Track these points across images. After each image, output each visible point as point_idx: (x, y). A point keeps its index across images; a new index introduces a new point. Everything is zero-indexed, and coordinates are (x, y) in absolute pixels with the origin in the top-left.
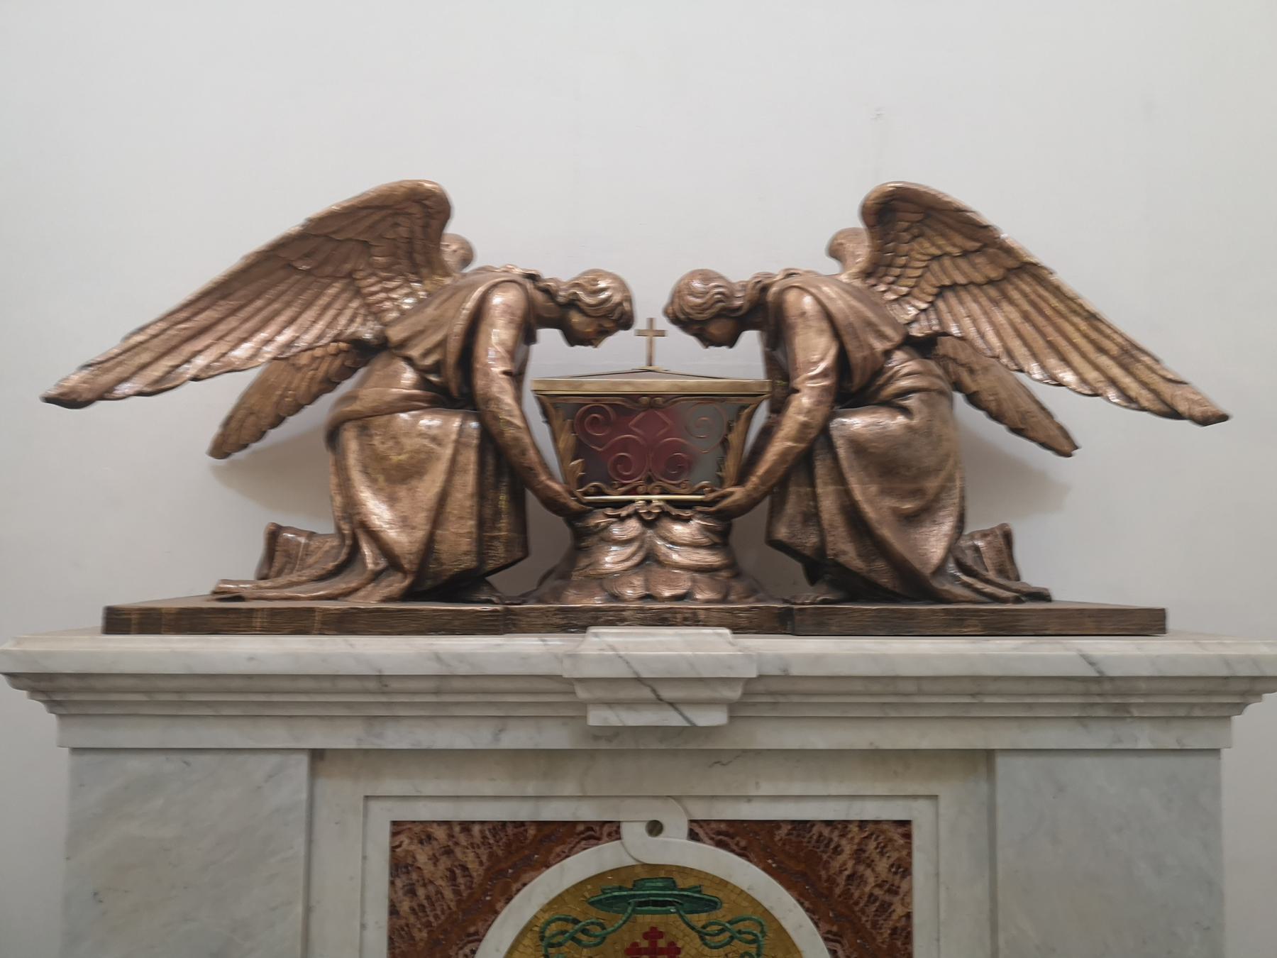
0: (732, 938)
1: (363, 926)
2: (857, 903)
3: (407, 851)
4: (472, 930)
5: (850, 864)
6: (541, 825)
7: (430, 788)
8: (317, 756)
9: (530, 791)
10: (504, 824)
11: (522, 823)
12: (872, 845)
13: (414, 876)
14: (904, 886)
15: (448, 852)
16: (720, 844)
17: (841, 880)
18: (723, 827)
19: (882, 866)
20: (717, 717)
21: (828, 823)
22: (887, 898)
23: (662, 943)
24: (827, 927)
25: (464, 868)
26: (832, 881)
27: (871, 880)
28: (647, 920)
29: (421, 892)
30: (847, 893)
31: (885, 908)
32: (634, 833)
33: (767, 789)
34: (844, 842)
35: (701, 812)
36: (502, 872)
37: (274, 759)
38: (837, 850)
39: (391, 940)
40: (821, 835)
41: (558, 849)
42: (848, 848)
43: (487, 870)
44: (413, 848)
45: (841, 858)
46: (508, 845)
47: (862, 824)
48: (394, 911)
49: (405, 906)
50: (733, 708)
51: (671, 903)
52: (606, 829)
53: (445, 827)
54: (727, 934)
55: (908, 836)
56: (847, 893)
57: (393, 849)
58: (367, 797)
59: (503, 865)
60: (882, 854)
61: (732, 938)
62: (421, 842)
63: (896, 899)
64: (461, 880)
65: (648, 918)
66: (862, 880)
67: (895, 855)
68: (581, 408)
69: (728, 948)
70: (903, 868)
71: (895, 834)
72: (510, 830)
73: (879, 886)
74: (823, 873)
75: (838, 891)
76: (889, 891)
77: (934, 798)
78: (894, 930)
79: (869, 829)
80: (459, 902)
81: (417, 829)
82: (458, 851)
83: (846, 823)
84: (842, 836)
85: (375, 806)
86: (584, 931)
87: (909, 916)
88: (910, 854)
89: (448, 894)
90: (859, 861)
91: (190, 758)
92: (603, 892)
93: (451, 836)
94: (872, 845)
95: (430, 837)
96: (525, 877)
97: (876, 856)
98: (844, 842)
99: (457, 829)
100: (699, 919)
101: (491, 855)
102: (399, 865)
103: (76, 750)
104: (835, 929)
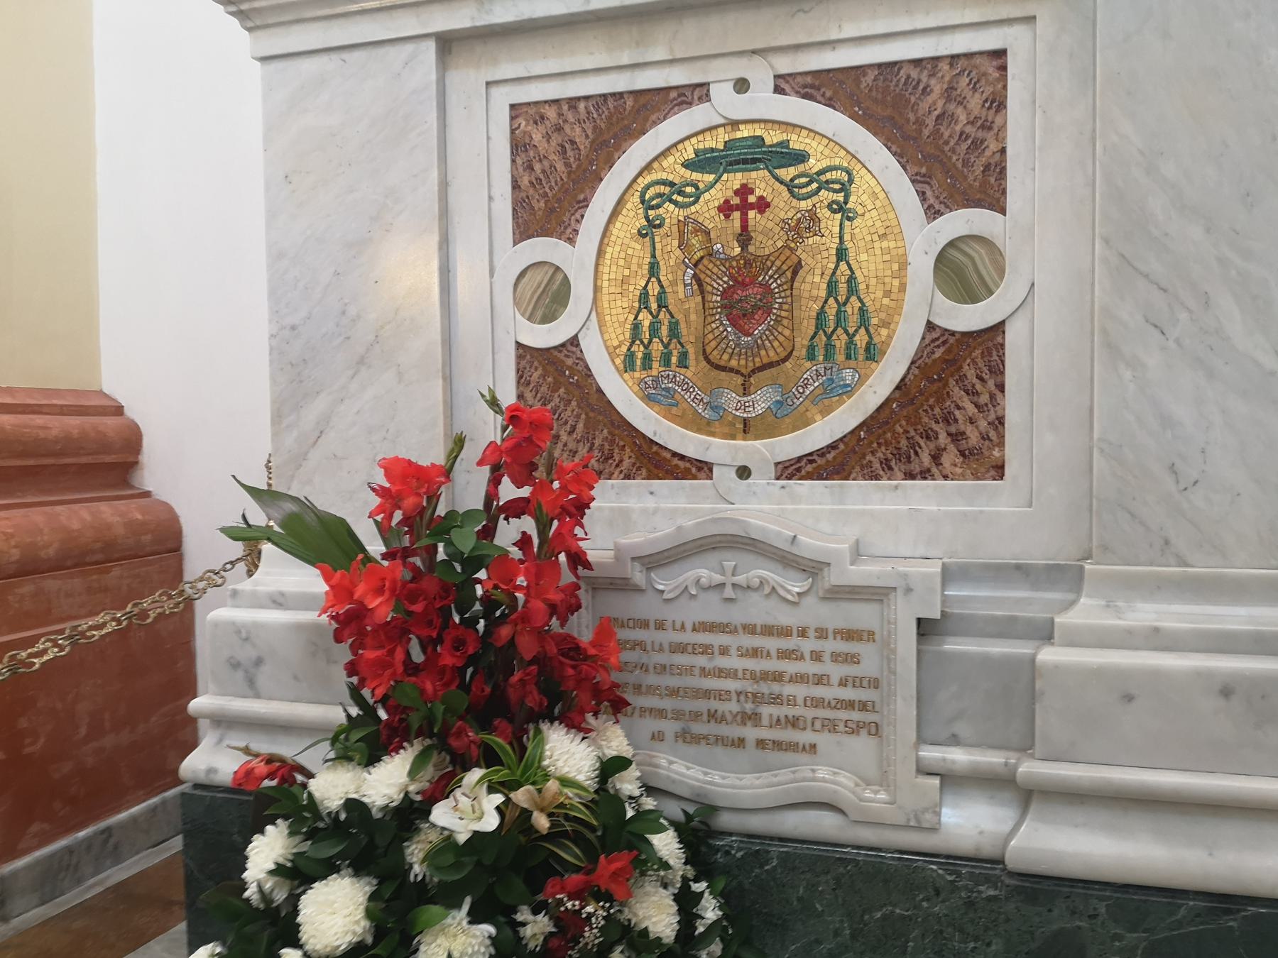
0: (819, 189)
1: (490, 198)
2: (947, 143)
3: (525, 132)
4: (581, 197)
5: (940, 104)
6: (637, 94)
7: (539, 68)
8: (447, 44)
9: (625, 60)
10: (604, 96)
11: (621, 94)
12: (964, 80)
13: (532, 153)
14: (998, 120)
15: (559, 129)
16: (806, 96)
17: (930, 121)
18: (809, 80)
19: (975, 102)
21: (917, 62)
22: (980, 134)
23: (752, 199)
24: (916, 169)
25: (573, 142)
26: (920, 123)
27: (963, 118)
28: (735, 180)
29: (537, 167)
30: (936, 134)
31: (977, 145)
32: (722, 94)
33: (850, 31)
34: (933, 82)
35: (785, 65)
36: (605, 143)
37: (409, 47)
38: (926, 91)
39: (514, 209)
40: (909, 77)
41: (654, 117)
42: (937, 88)
43: (592, 142)
44: (529, 128)
45: (930, 99)
46: (609, 118)
47: (954, 58)
48: (516, 186)
49: (525, 181)
51: (759, 160)
52: (697, 93)
53: (554, 107)
54: (815, 185)
55: (1003, 68)
56: (936, 134)
57: (513, 131)
58: (488, 84)
59: (606, 137)
60: (974, 89)
61: (819, 189)
62: (536, 123)
63: (990, 136)
64: (570, 153)
65: (739, 175)
66: (953, 118)
67: (989, 90)
68: (877, 423)
69: (815, 199)
70: (998, 103)
71: (990, 67)
72: (611, 103)
73: (972, 123)
74: (912, 117)
75: (926, 132)
76: (983, 127)
77: (1031, 19)
78: (987, 167)
79: (961, 64)
80: (569, 173)
81: (532, 111)
82: (567, 128)
83: (936, 59)
84: (931, 75)
85: (495, 91)
86: (680, 193)
87: (1003, 151)
88: (1005, 87)
89: (560, 166)
90: (949, 99)
91: (346, 55)
92: (697, 152)
93: (560, 115)
94: (964, 80)
95: (542, 118)
96: (624, 145)
97: (968, 93)
98: (933, 82)
99: (565, 107)
100: (787, 173)
101: (595, 128)
102: (518, 146)
103: (264, 59)
104: (924, 170)
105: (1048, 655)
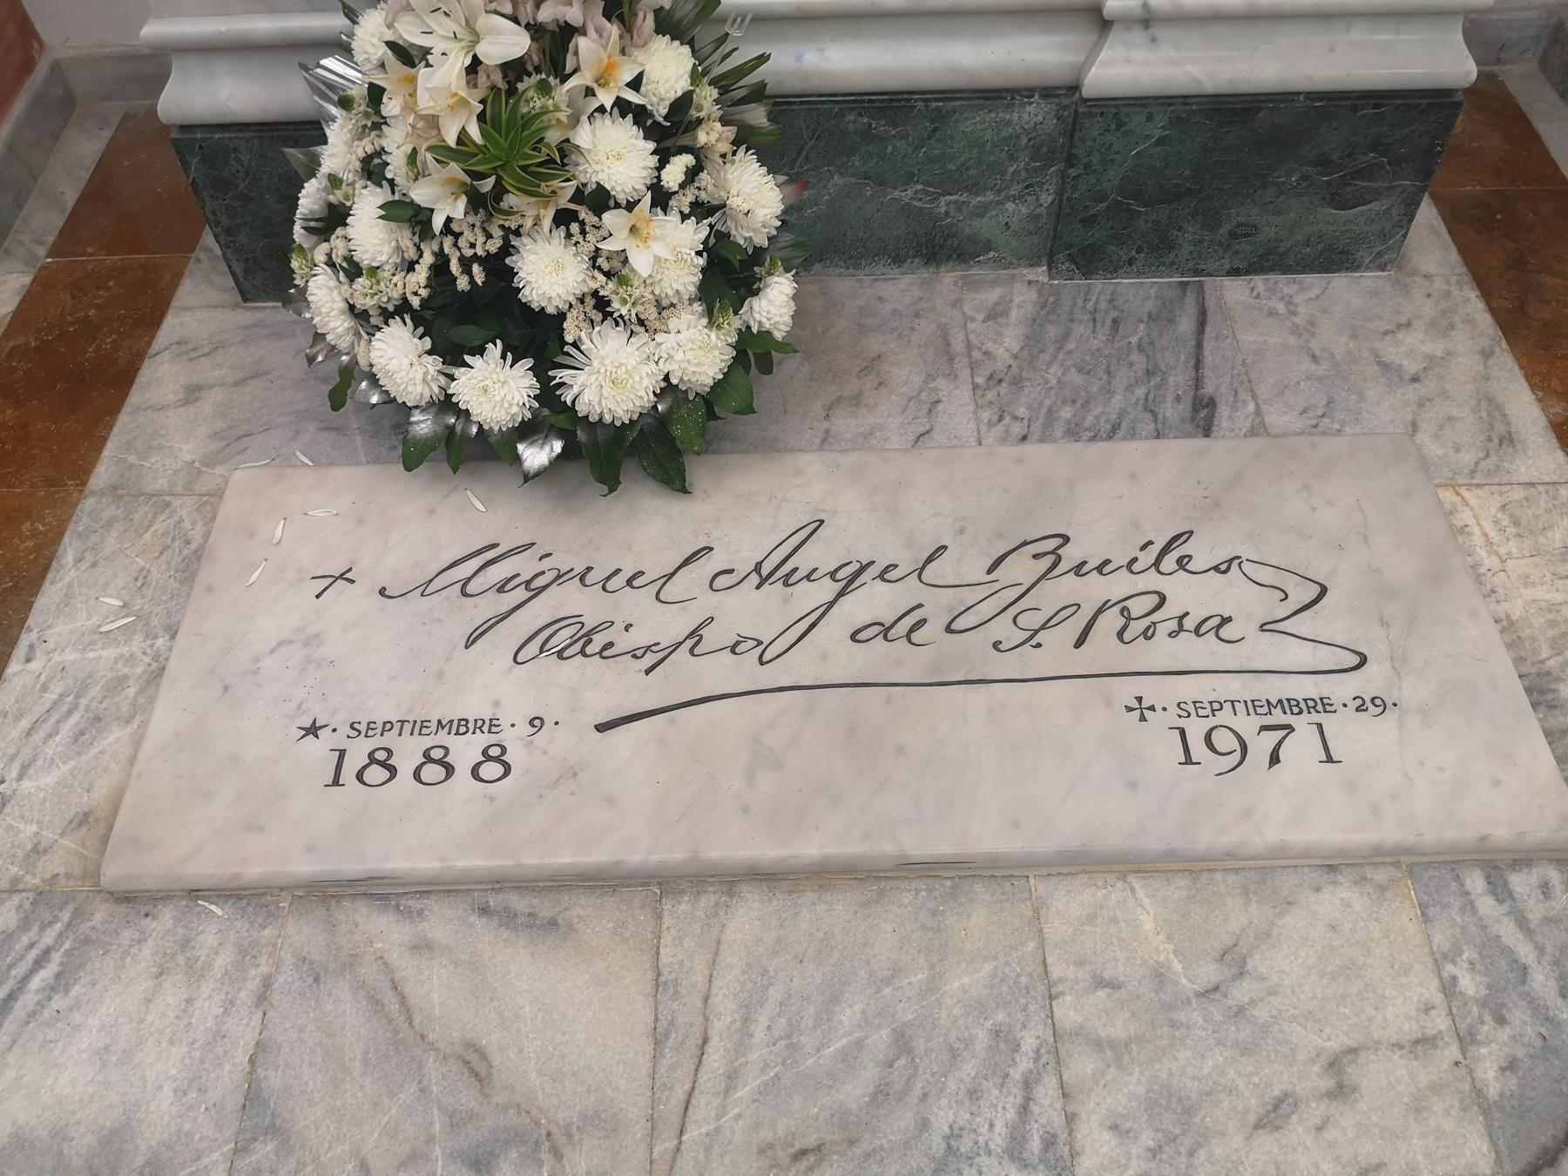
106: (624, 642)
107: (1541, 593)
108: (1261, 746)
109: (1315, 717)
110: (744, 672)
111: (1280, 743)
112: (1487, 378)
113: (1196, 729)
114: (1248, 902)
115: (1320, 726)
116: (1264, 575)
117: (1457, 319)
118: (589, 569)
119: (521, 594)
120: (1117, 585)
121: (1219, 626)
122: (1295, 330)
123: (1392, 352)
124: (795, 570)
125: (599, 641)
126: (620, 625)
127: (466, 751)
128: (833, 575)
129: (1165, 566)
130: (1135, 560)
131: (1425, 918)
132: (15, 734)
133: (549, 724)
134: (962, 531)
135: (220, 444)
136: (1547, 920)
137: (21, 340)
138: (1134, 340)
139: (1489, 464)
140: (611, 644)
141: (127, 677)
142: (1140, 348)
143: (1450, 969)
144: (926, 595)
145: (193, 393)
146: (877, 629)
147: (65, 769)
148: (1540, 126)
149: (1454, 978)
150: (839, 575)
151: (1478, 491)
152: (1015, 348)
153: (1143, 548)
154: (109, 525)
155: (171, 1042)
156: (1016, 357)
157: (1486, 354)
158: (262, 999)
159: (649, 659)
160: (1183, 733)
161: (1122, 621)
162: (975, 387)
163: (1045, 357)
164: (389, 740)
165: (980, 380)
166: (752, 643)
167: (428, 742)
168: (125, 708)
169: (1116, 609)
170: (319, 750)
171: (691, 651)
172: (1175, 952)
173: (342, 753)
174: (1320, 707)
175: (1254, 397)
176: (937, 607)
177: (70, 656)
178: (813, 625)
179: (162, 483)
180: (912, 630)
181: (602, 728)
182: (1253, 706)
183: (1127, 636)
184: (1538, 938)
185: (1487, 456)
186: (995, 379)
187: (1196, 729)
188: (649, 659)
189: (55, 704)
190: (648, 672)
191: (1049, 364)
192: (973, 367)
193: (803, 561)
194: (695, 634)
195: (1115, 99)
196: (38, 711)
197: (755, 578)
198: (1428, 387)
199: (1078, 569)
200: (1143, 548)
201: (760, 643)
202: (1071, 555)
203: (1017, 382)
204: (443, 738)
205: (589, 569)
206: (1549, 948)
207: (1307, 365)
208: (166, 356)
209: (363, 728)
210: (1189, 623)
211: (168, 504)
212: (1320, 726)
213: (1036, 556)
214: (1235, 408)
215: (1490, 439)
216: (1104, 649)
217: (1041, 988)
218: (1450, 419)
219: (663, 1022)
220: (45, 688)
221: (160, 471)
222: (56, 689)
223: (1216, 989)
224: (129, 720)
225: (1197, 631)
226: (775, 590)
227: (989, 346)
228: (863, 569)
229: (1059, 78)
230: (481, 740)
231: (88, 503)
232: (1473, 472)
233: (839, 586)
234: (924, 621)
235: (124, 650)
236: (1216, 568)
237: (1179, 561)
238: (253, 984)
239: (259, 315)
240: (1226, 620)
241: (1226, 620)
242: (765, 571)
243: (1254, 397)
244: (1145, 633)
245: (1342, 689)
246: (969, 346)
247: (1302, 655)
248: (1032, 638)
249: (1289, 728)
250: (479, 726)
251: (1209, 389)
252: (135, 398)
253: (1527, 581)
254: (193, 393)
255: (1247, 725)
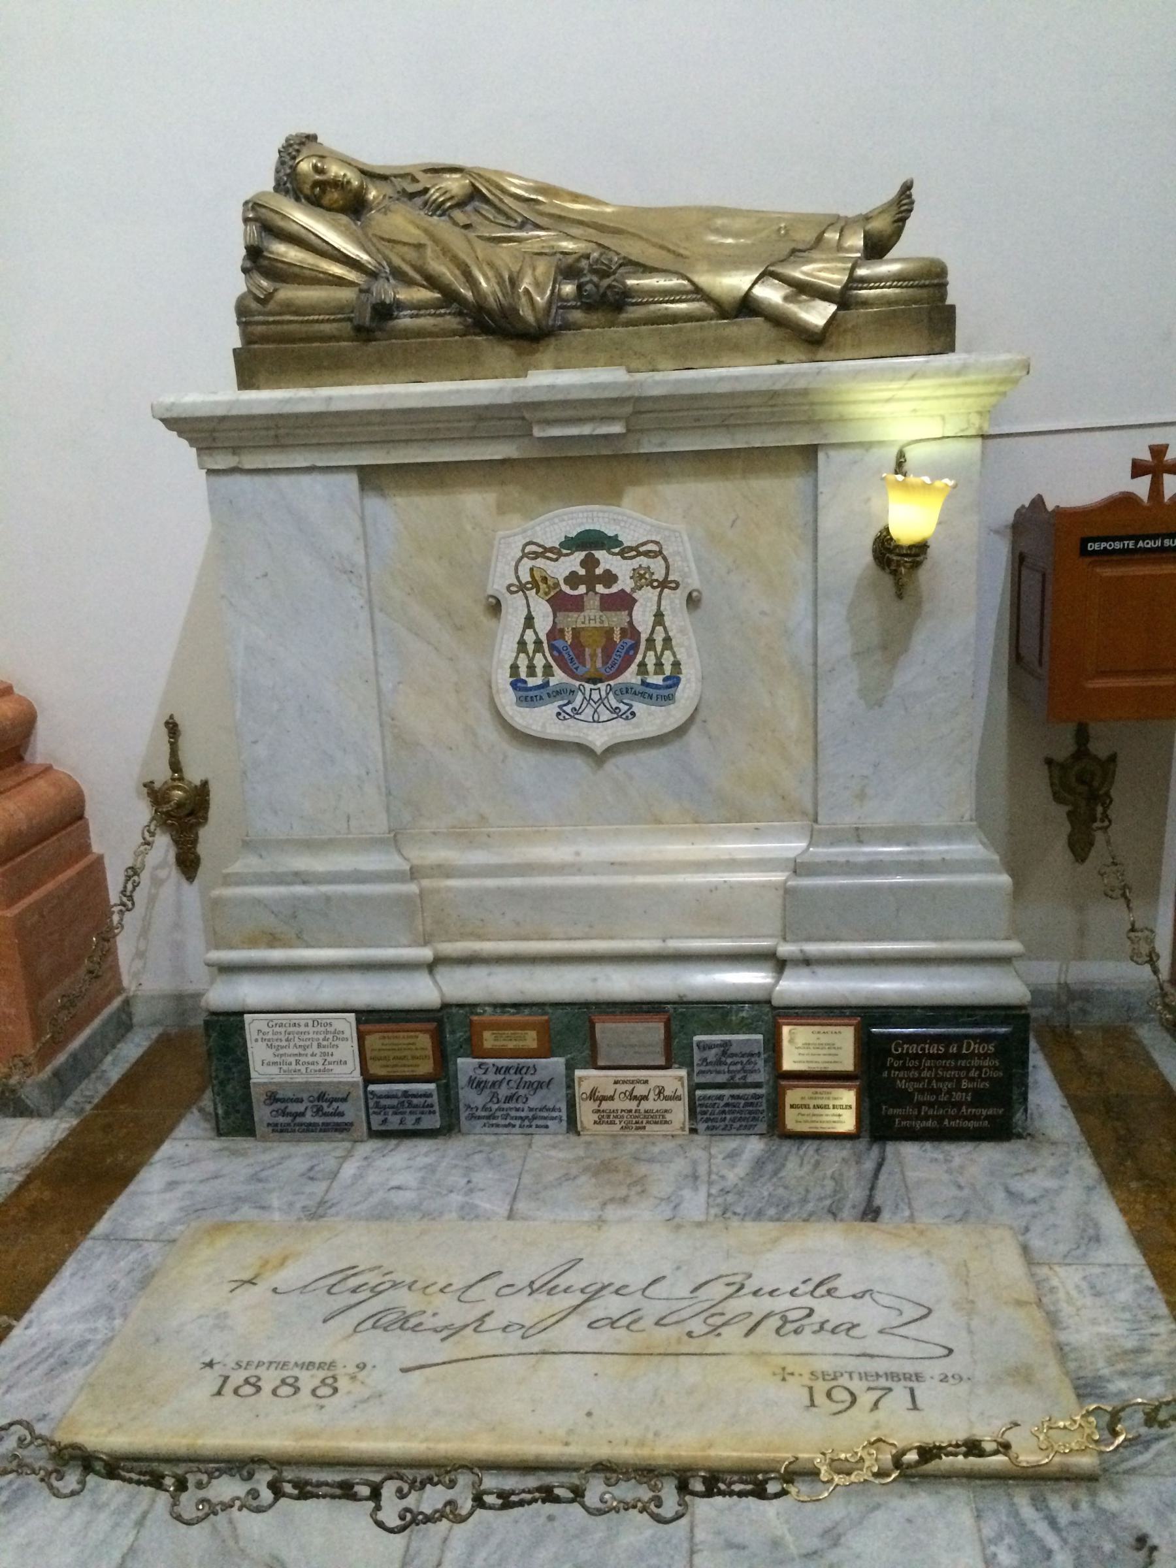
20: (617, 428)
50: (627, 420)
105: (794, 846)
106: (430, 1322)
107: (1103, 1329)
108: (866, 1399)
109: (910, 1384)
110: (513, 1341)
111: (881, 1398)
112: (1086, 1203)
113: (821, 1387)
114: (849, 1502)
115: (912, 1391)
116: (886, 1300)
117: (1071, 1169)
118: (416, 1282)
119: (368, 1294)
120: (783, 1302)
121: (849, 1329)
122: (949, 1171)
123: (1017, 1185)
124: (557, 1286)
125: (413, 1322)
126: (430, 1312)
127: (308, 1380)
128: (582, 1291)
129: (817, 1293)
130: (797, 1289)
131: (978, 1517)
132: (8, 1369)
133: (369, 1367)
134: (678, 1268)
135: (182, 1214)
136: (1073, 1523)
137: (65, 1154)
138: (829, 1173)
139: (1079, 1252)
140: (421, 1324)
141: (89, 1341)
142: (833, 1178)
143: (993, 1548)
144: (644, 1303)
145: (172, 1185)
146: (608, 1321)
147: (36, 1390)
148: (1156, 1056)
149: (995, 1555)
150: (588, 1290)
151: (1068, 1268)
152: (742, 1174)
153: (804, 1282)
154: (99, 1256)
155: (72, 1545)
156: (742, 1179)
157: (1089, 1189)
158: (140, 1523)
159: (444, 1334)
160: (811, 1389)
161: (780, 1323)
162: (709, 1195)
163: (763, 1180)
164: (260, 1372)
165: (713, 1191)
166: (517, 1327)
167: (286, 1373)
168: (84, 1359)
169: (777, 1317)
170: (211, 1379)
171: (475, 1330)
172: (789, 1530)
173: (226, 1378)
174: (914, 1378)
175: (910, 1207)
176: (653, 1310)
177: (55, 1327)
178: (561, 1319)
179: (140, 1235)
180: (631, 1323)
181: (404, 1370)
182: (864, 1376)
183: (782, 1332)
184: (1064, 1534)
185: (1078, 1247)
186: (725, 1192)
187: (821, 1387)
188: (444, 1334)
189: (38, 1354)
190: (443, 1340)
191: (764, 1185)
192: (710, 1184)
193: (563, 1282)
194: (482, 1319)
195: (795, 1008)
196: (24, 1358)
197: (528, 1290)
198: (1044, 1205)
199: (755, 1293)
200: (804, 1282)
201: (523, 1326)
202: (752, 1285)
203: (740, 1194)
204: (296, 1372)
205: (416, 1282)
206: (1071, 1540)
207: (954, 1192)
208: (158, 1165)
209: (244, 1365)
210: (828, 1326)
211: (140, 1246)
212: (912, 1391)
213: (728, 1285)
214: (894, 1213)
215: (1082, 1238)
216: (765, 1334)
217: (686, 1545)
218: (1055, 1226)
219: (412, 1552)
220: (34, 1344)
221: (141, 1226)
222: (43, 1344)
223: (815, 1553)
224: (86, 1364)
225: (833, 1331)
226: (542, 1297)
227: (725, 1172)
228: (603, 1288)
229: (761, 996)
230: (321, 1374)
231: (88, 1243)
232: (1065, 1256)
233: (585, 1297)
234: (640, 1318)
235: (92, 1325)
236: (854, 1296)
237: (829, 1292)
238: (134, 1516)
239: (226, 1145)
240: (854, 1326)
241: (854, 1326)
242: (535, 1286)
243: (910, 1207)
244: (796, 1332)
245: (934, 1369)
246: (710, 1173)
247: (909, 1349)
248: (715, 1330)
249: (890, 1390)
250: (321, 1366)
251: (878, 1202)
252: (132, 1188)
253: (1094, 1322)
254: (172, 1185)
255: (856, 1385)
